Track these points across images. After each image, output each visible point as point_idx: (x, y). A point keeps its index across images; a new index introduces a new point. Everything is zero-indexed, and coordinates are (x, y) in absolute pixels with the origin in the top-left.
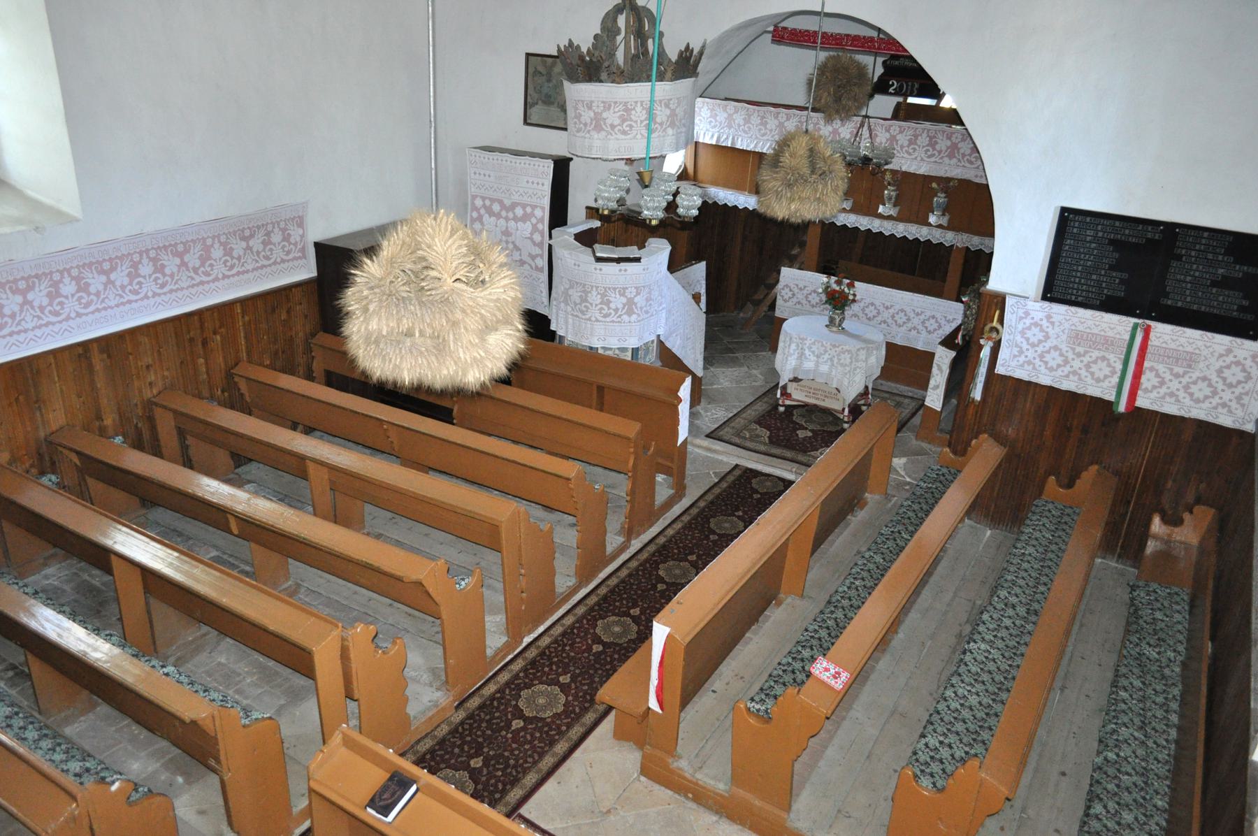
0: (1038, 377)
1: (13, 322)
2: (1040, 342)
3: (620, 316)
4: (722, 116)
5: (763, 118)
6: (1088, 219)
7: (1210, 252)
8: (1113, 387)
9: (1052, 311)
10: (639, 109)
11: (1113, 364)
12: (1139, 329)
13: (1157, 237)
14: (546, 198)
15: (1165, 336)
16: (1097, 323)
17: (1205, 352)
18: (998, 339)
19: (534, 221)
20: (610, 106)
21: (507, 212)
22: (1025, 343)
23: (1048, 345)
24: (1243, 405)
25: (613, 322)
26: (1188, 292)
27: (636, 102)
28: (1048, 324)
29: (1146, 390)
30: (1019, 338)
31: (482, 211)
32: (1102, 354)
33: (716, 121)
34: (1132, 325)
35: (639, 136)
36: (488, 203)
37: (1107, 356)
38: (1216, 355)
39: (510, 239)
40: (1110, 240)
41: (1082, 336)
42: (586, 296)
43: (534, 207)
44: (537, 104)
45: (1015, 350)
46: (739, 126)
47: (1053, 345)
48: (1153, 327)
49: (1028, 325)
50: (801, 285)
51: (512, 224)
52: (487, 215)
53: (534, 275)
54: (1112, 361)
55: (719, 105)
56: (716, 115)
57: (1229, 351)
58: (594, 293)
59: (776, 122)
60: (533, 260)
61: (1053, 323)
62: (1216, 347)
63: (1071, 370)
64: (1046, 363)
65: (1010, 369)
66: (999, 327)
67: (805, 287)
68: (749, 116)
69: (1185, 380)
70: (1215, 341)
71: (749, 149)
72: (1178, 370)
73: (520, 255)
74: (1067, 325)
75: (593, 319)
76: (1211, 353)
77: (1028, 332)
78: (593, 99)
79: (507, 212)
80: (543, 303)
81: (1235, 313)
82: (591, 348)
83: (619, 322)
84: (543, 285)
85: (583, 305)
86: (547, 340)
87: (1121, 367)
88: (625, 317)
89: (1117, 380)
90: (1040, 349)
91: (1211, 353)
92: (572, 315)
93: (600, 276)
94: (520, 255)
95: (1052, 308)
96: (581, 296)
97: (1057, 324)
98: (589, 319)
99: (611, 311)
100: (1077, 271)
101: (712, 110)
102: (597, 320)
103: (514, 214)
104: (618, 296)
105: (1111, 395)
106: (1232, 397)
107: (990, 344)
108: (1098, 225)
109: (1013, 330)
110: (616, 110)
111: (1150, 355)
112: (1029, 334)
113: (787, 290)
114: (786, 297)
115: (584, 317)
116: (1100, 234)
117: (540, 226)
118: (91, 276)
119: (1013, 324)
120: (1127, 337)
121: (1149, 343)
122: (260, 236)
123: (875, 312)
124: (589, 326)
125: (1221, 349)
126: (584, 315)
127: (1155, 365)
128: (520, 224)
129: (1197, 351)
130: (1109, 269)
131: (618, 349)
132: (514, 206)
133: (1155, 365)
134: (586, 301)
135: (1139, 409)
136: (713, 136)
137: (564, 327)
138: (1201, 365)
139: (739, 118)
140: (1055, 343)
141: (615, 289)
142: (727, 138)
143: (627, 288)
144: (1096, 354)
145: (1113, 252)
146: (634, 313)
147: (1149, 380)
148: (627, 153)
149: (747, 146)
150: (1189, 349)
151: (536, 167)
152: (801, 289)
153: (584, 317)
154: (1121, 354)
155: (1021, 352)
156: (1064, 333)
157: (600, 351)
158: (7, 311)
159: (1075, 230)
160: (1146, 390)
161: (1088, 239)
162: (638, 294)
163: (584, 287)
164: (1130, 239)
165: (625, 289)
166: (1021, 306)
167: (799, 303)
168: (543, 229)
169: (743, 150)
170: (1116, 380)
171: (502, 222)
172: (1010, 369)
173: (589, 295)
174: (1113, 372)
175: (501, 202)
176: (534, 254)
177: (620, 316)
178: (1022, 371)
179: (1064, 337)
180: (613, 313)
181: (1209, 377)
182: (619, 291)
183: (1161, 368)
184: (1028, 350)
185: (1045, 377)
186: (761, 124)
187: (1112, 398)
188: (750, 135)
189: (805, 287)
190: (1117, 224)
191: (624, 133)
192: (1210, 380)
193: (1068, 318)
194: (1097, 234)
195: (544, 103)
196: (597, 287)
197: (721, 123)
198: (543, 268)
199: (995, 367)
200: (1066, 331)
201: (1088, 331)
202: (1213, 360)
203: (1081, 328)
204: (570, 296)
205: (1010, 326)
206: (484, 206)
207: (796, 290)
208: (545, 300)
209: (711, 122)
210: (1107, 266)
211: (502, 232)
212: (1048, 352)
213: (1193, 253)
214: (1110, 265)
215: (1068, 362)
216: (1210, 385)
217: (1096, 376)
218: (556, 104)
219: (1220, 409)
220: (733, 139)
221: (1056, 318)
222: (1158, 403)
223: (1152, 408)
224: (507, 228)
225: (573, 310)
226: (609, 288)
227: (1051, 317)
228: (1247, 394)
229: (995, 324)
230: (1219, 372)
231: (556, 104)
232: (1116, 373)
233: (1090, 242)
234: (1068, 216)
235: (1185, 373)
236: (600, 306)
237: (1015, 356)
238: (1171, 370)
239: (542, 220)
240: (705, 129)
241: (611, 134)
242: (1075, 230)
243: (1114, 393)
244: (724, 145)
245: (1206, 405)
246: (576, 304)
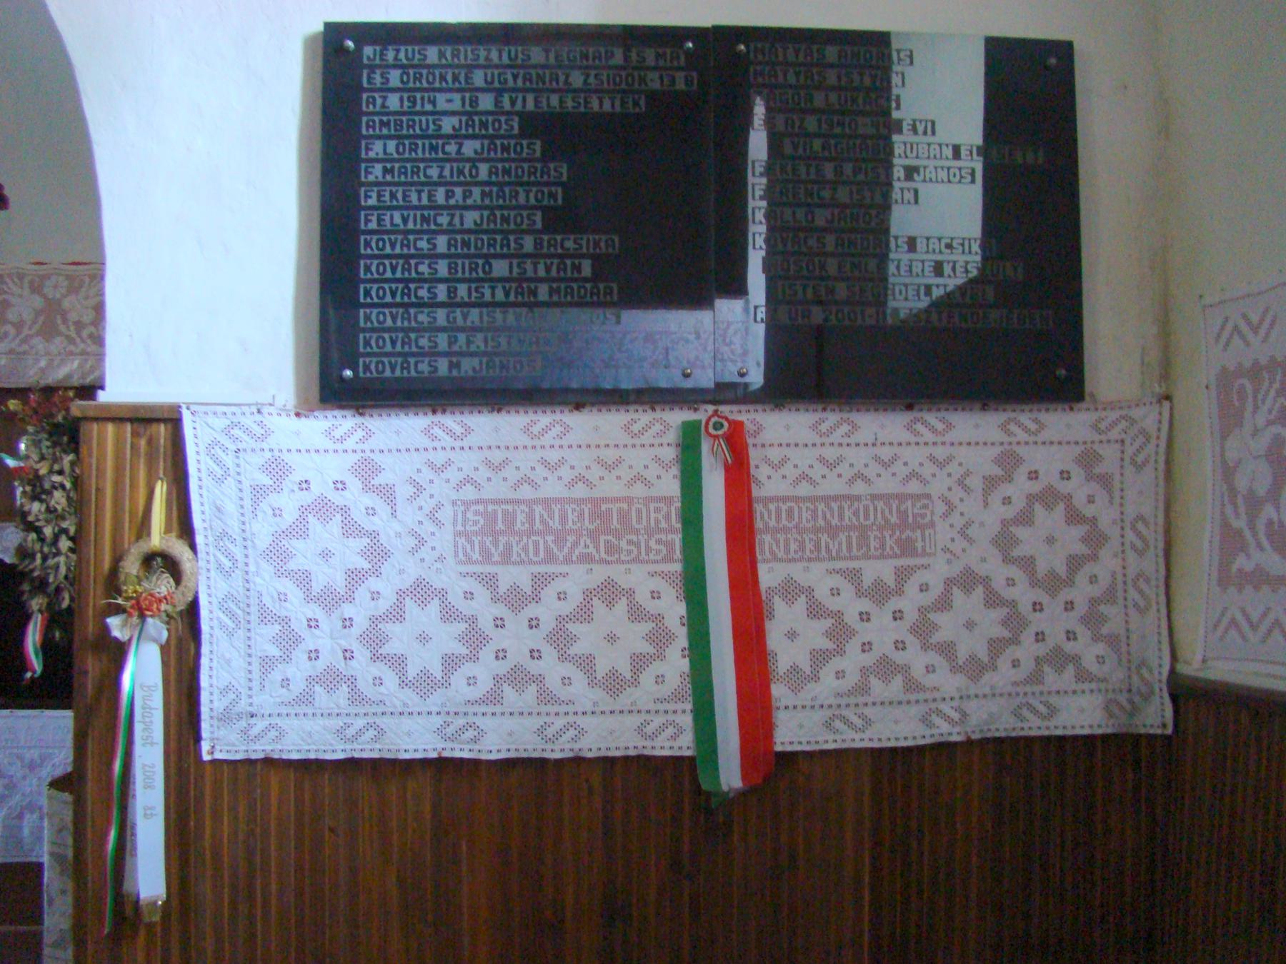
0: (381, 732)
2: (355, 577)
6: (432, 54)
7: (862, 113)
8: (676, 696)
9: (372, 443)
11: (652, 606)
12: (705, 446)
13: (681, 85)
15: (795, 455)
16: (553, 456)
17: (938, 486)
18: (181, 603)
22: (295, 595)
23: (387, 585)
24: (1112, 641)
26: (832, 266)
28: (368, 500)
29: (797, 678)
30: (266, 581)
32: (600, 573)
34: (672, 436)
37: (624, 581)
38: (976, 483)
40: (525, 117)
41: (510, 519)
45: (265, 640)
47: (407, 582)
48: (749, 426)
49: (290, 517)
54: (822, 593)
57: (1009, 461)
61: (387, 493)
62: (962, 453)
63: (868, 659)
64: (398, 663)
65: (260, 725)
66: (179, 549)
69: (910, 602)
70: (864, 435)
72: (879, 570)
74: (441, 490)
76: (961, 483)
77: (299, 545)
81: (994, 314)
87: (681, 609)
89: (685, 665)
90: (360, 611)
91: (961, 483)
95: (369, 434)
97: (404, 491)
100: (434, 257)
105: (681, 731)
106: (535, 639)
107: (157, 628)
108: (470, 68)
109: (238, 552)
111: (767, 538)
112: (303, 554)
116: (486, 102)
119: (234, 526)
120: (671, 486)
121: (755, 492)
122: (1261, 420)
123: (1049, 520)
125: (982, 462)
127: (796, 571)
129: (914, 487)
130: (547, 228)
133: (796, 571)
135: (788, 758)
138: (943, 533)
140: (413, 571)
144: (576, 580)
145: (545, 158)
147: (792, 635)
150: (887, 485)
154: (669, 559)
155: (289, 641)
156: (438, 523)
158: (11, 315)
159: (393, 102)
160: (797, 678)
161: (448, 125)
164: (595, 105)
166: (248, 442)
170: (676, 664)
172: (260, 725)
174: (660, 639)
178: (308, 724)
179: (444, 540)
181: (982, 569)
183: (818, 578)
184: (865, 617)
185: (407, 723)
187: (684, 745)
190: (537, 55)
192: (442, 594)
193: (440, 458)
194: (474, 102)
199: (198, 738)
200: (446, 514)
201: (526, 492)
202: (970, 507)
203: (496, 489)
205: (224, 534)
210: (538, 217)
212: (943, 604)
213: (811, 124)
214: (544, 209)
215: (483, 640)
216: (993, 600)
217: (962, 654)
219: (1052, 679)
221: (394, 471)
222: (850, 714)
223: (830, 742)
227: (378, 470)
228: (1110, 596)
229: (158, 538)
230: (1004, 542)
232: (669, 637)
233: (456, 136)
234: (359, 48)
235: (902, 575)
237: (267, 664)
238: (854, 576)
242: (393, 102)
243: (687, 721)
245: (1003, 676)
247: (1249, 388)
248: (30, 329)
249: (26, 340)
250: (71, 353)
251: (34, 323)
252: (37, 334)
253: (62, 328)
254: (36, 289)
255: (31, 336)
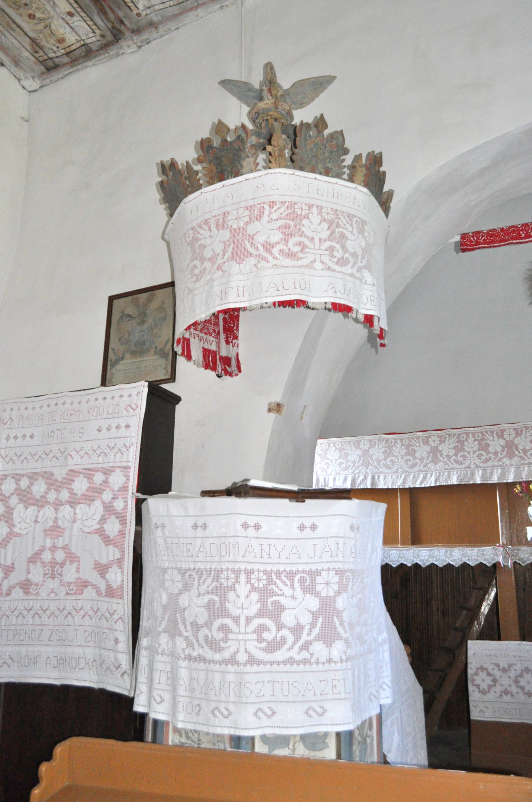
1: (294, 643)
3: (306, 646)
4: (354, 454)
5: (408, 446)
10: (315, 217)
14: (132, 449)
19: (107, 496)
20: (262, 211)
21: (58, 492)
25: (290, 661)
27: (310, 206)
31: (14, 501)
33: (348, 461)
35: (318, 265)
36: (24, 483)
39: (60, 542)
42: (224, 599)
43: (107, 471)
44: (123, 358)
46: (379, 462)
50: (504, 664)
51: (66, 511)
52: (21, 506)
53: (104, 607)
55: (349, 442)
56: (347, 454)
58: (243, 588)
59: (428, 448)
60: (103, 575)
67: (510, 666)
68: (390, 448)
71: (395, 487)
73: (78, 570)
75: (242, 657)
78: (228, 209)
79: (58, 492)
80: (119, 666)
82: (236, 741)
83: (305, 661)
84: (120, 626)
85: (217, 624)
86: (124, 739)
88: (318, 648)
92: (189, 658)
93: (255, 543)
94: (78, 570)
96: (209, 606)
98: (233, 661)
99: (285, 632)
101: (341, 450)
102: (252, 661)
103: (71, 490)
104: (299, 592)
110: (274, 216)
113: (483, 675)
114: (484, 686)
115: (217, 657)
117: (119, 504)
118: (288, 591)
124: (231, 678)
126: (220, 650)
128: (81, 508)
131: (304, 738)
132: (72, 475)
134: (224, 612)
136: (345, 479)
137: (167, 696)
139: (377, 452)
141: (291, 575)
142: (365, 478)
143: (318, 573)
146: (339, 637)
148: (298, 291)
149: (393, 483)
151: (117, 399)
152: (504, 670)
153: (217, 657)
157: (260, 748)
162: (342, 589)
163: (217, 578)
165: (314, 574)
167: (506, 692)
168: (125, 508)
169: (388, 490)
171: (48, 512)
173: (231, 596)
175: (48, 476)
176: (104, 562)
177: (306, 646)
180: (290, 638)
182: (302, 581)
186: (408, 454)
188: (394, 470)
189: (510, 666)
191: (292, 255)
195: (134, 354)
196: (249, 573)
197: (354, 462)
198: (121, 588)
204: (182, 611)
206: (18, 491)
207: (497, 673)
208: (124, 659)
209: (340, 464)
211: (45, 531)
218: (152, 351)
220: (373, 478)
224: (56, 520)
225: (190, 644)
226: (279, 574)
231: (152, 351)
236: (257, 622)
239: (122, 492)
240: (333, 473)
241: (266, 259)
244: (362, 487)
246: (196, 627)
247: (351, 577)
248: (502, 454)
249: (425, 466)
250: (523, 464)
251: (428, 457)
252: (506, 457)
253: (441, 459)
254: (501, 435)
255: (502, 458)
